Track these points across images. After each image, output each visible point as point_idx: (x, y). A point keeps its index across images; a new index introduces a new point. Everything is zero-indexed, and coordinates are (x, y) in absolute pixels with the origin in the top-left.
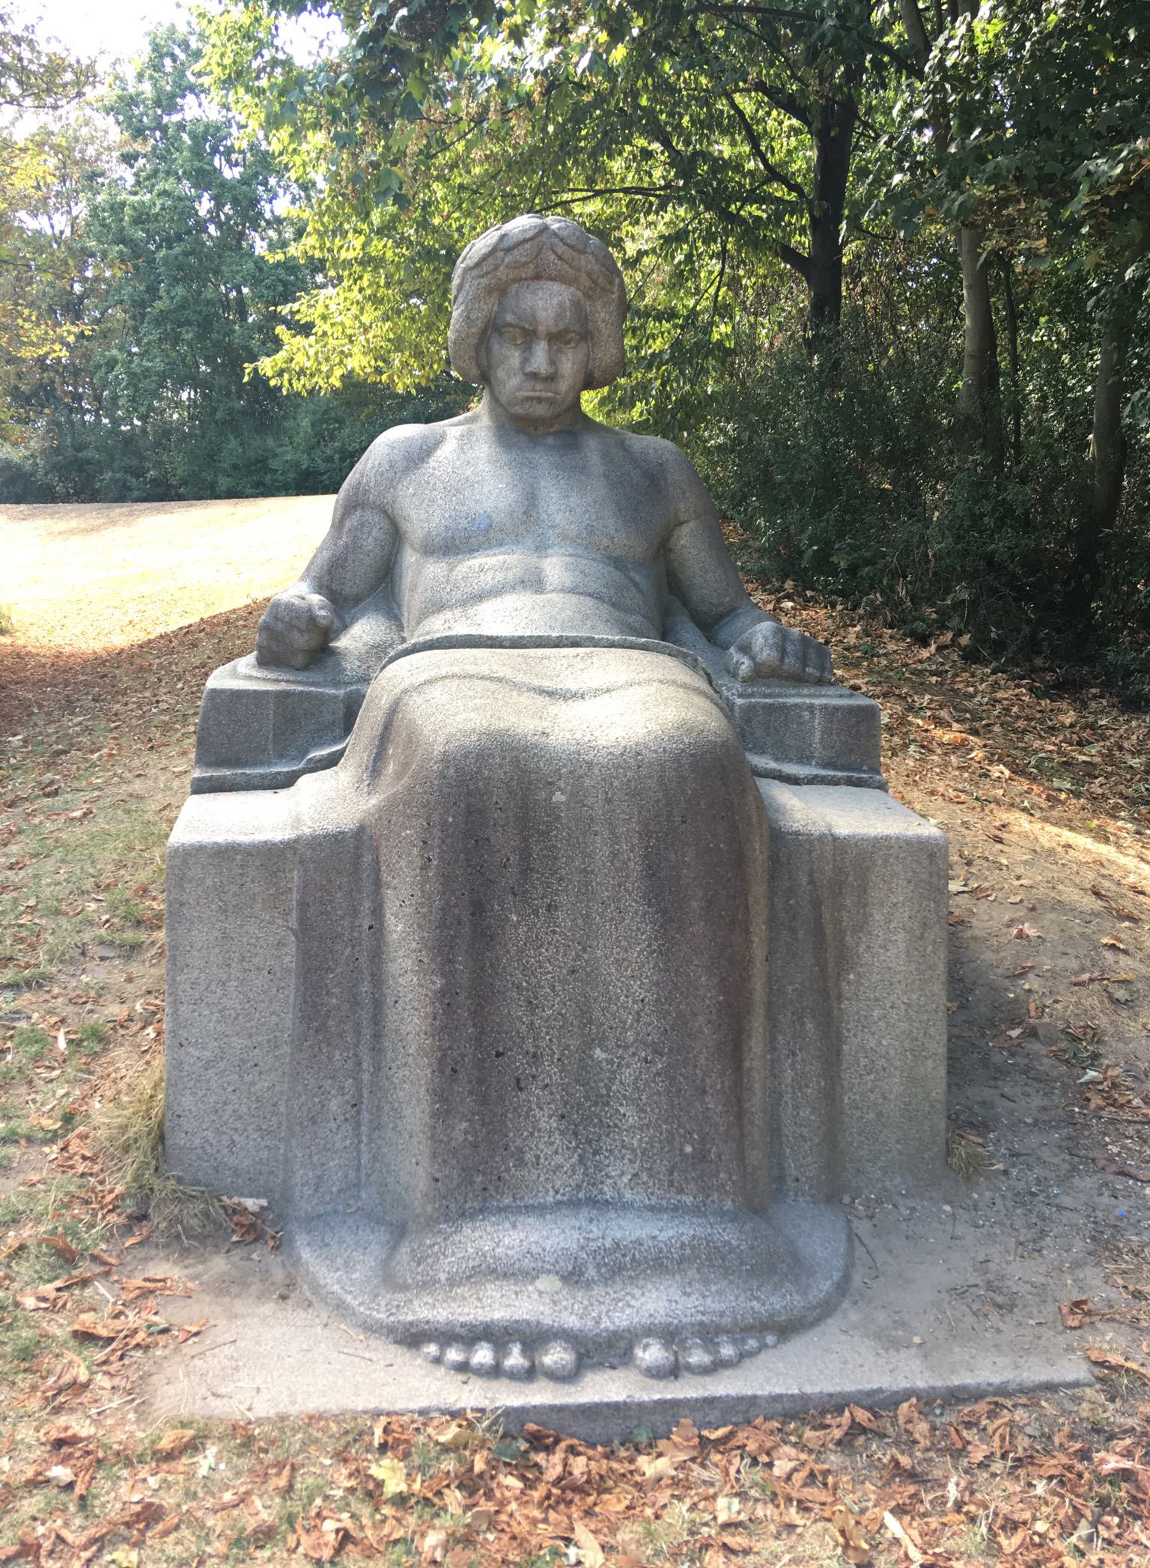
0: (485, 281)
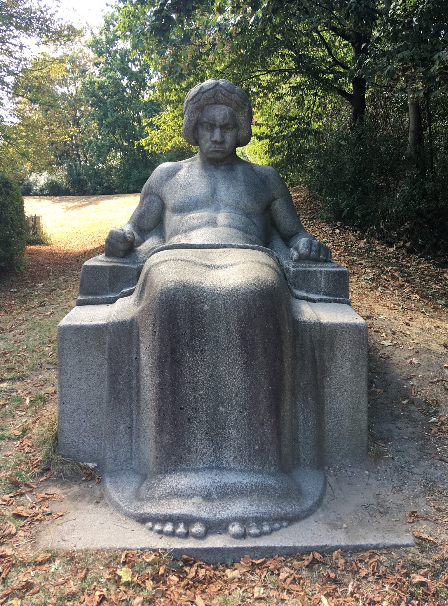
0: (195, 105)
